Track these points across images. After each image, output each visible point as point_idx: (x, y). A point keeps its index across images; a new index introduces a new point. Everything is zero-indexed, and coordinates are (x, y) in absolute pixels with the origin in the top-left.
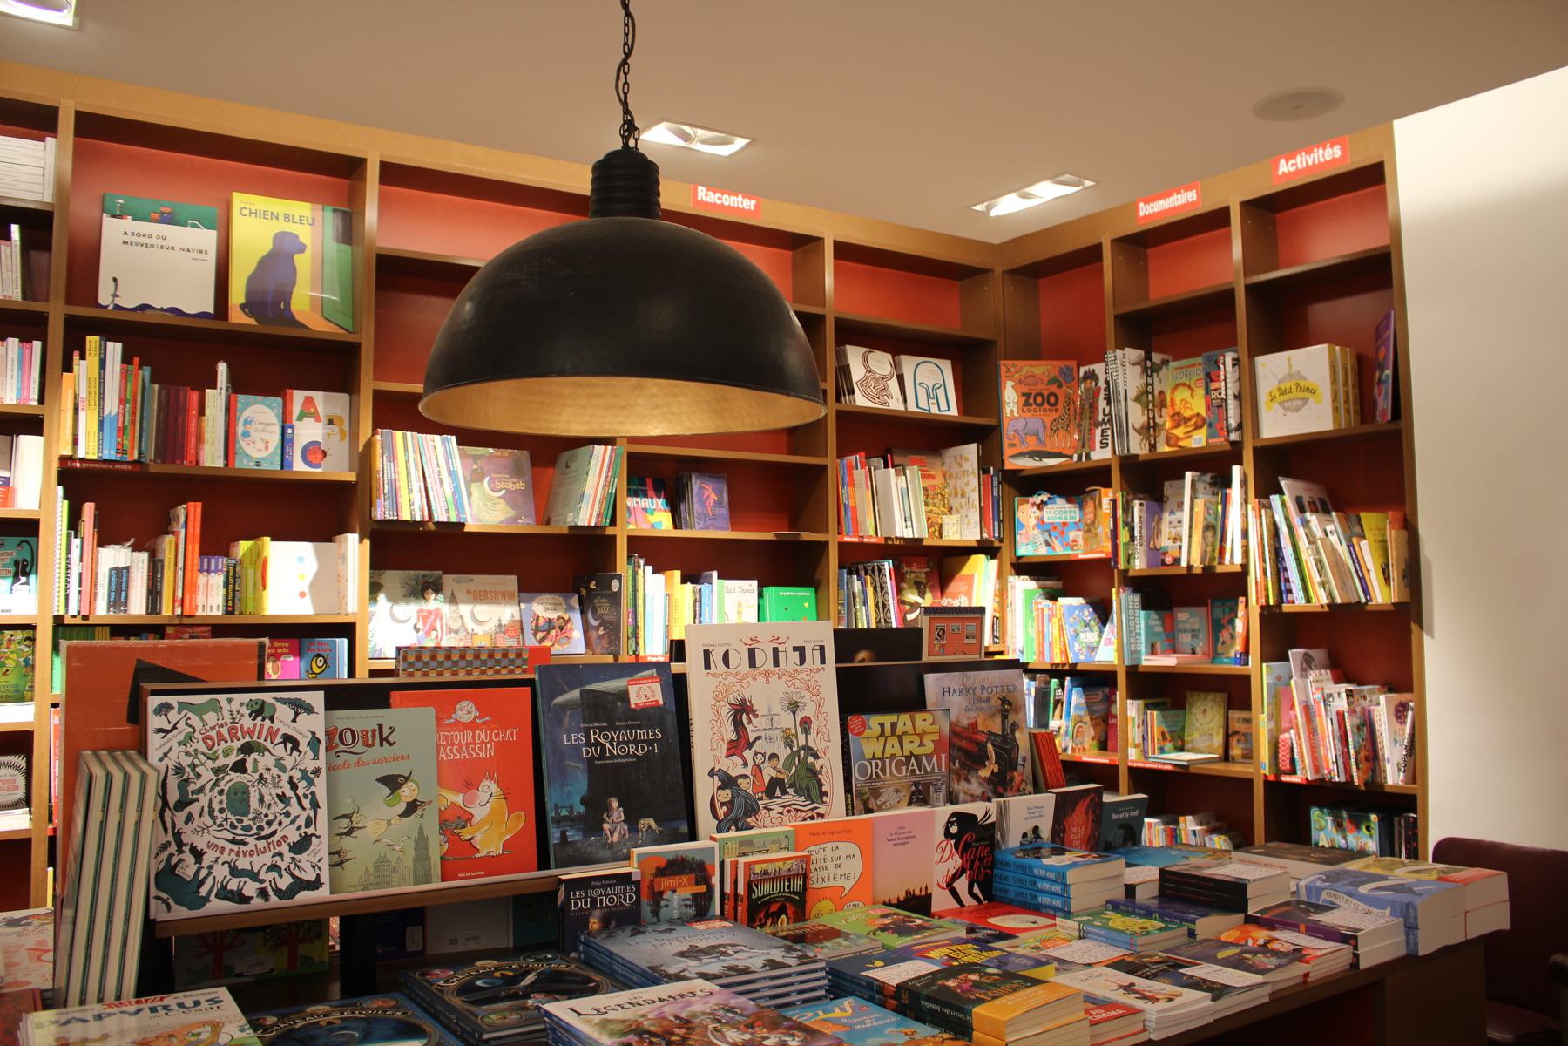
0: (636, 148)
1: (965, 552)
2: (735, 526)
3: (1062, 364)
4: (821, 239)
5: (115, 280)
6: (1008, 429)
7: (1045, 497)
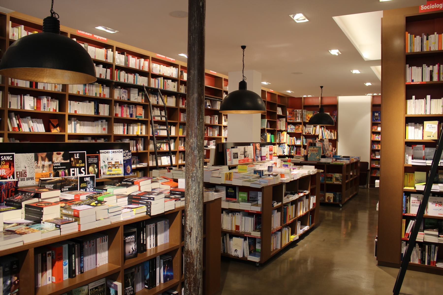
0: (55, 17)
1: (282, 131)
2: (270, 128)
3: (293, 109)
4: (149, 57)
5: (322, 87)
6: (288, 117)
7: (291, 125)
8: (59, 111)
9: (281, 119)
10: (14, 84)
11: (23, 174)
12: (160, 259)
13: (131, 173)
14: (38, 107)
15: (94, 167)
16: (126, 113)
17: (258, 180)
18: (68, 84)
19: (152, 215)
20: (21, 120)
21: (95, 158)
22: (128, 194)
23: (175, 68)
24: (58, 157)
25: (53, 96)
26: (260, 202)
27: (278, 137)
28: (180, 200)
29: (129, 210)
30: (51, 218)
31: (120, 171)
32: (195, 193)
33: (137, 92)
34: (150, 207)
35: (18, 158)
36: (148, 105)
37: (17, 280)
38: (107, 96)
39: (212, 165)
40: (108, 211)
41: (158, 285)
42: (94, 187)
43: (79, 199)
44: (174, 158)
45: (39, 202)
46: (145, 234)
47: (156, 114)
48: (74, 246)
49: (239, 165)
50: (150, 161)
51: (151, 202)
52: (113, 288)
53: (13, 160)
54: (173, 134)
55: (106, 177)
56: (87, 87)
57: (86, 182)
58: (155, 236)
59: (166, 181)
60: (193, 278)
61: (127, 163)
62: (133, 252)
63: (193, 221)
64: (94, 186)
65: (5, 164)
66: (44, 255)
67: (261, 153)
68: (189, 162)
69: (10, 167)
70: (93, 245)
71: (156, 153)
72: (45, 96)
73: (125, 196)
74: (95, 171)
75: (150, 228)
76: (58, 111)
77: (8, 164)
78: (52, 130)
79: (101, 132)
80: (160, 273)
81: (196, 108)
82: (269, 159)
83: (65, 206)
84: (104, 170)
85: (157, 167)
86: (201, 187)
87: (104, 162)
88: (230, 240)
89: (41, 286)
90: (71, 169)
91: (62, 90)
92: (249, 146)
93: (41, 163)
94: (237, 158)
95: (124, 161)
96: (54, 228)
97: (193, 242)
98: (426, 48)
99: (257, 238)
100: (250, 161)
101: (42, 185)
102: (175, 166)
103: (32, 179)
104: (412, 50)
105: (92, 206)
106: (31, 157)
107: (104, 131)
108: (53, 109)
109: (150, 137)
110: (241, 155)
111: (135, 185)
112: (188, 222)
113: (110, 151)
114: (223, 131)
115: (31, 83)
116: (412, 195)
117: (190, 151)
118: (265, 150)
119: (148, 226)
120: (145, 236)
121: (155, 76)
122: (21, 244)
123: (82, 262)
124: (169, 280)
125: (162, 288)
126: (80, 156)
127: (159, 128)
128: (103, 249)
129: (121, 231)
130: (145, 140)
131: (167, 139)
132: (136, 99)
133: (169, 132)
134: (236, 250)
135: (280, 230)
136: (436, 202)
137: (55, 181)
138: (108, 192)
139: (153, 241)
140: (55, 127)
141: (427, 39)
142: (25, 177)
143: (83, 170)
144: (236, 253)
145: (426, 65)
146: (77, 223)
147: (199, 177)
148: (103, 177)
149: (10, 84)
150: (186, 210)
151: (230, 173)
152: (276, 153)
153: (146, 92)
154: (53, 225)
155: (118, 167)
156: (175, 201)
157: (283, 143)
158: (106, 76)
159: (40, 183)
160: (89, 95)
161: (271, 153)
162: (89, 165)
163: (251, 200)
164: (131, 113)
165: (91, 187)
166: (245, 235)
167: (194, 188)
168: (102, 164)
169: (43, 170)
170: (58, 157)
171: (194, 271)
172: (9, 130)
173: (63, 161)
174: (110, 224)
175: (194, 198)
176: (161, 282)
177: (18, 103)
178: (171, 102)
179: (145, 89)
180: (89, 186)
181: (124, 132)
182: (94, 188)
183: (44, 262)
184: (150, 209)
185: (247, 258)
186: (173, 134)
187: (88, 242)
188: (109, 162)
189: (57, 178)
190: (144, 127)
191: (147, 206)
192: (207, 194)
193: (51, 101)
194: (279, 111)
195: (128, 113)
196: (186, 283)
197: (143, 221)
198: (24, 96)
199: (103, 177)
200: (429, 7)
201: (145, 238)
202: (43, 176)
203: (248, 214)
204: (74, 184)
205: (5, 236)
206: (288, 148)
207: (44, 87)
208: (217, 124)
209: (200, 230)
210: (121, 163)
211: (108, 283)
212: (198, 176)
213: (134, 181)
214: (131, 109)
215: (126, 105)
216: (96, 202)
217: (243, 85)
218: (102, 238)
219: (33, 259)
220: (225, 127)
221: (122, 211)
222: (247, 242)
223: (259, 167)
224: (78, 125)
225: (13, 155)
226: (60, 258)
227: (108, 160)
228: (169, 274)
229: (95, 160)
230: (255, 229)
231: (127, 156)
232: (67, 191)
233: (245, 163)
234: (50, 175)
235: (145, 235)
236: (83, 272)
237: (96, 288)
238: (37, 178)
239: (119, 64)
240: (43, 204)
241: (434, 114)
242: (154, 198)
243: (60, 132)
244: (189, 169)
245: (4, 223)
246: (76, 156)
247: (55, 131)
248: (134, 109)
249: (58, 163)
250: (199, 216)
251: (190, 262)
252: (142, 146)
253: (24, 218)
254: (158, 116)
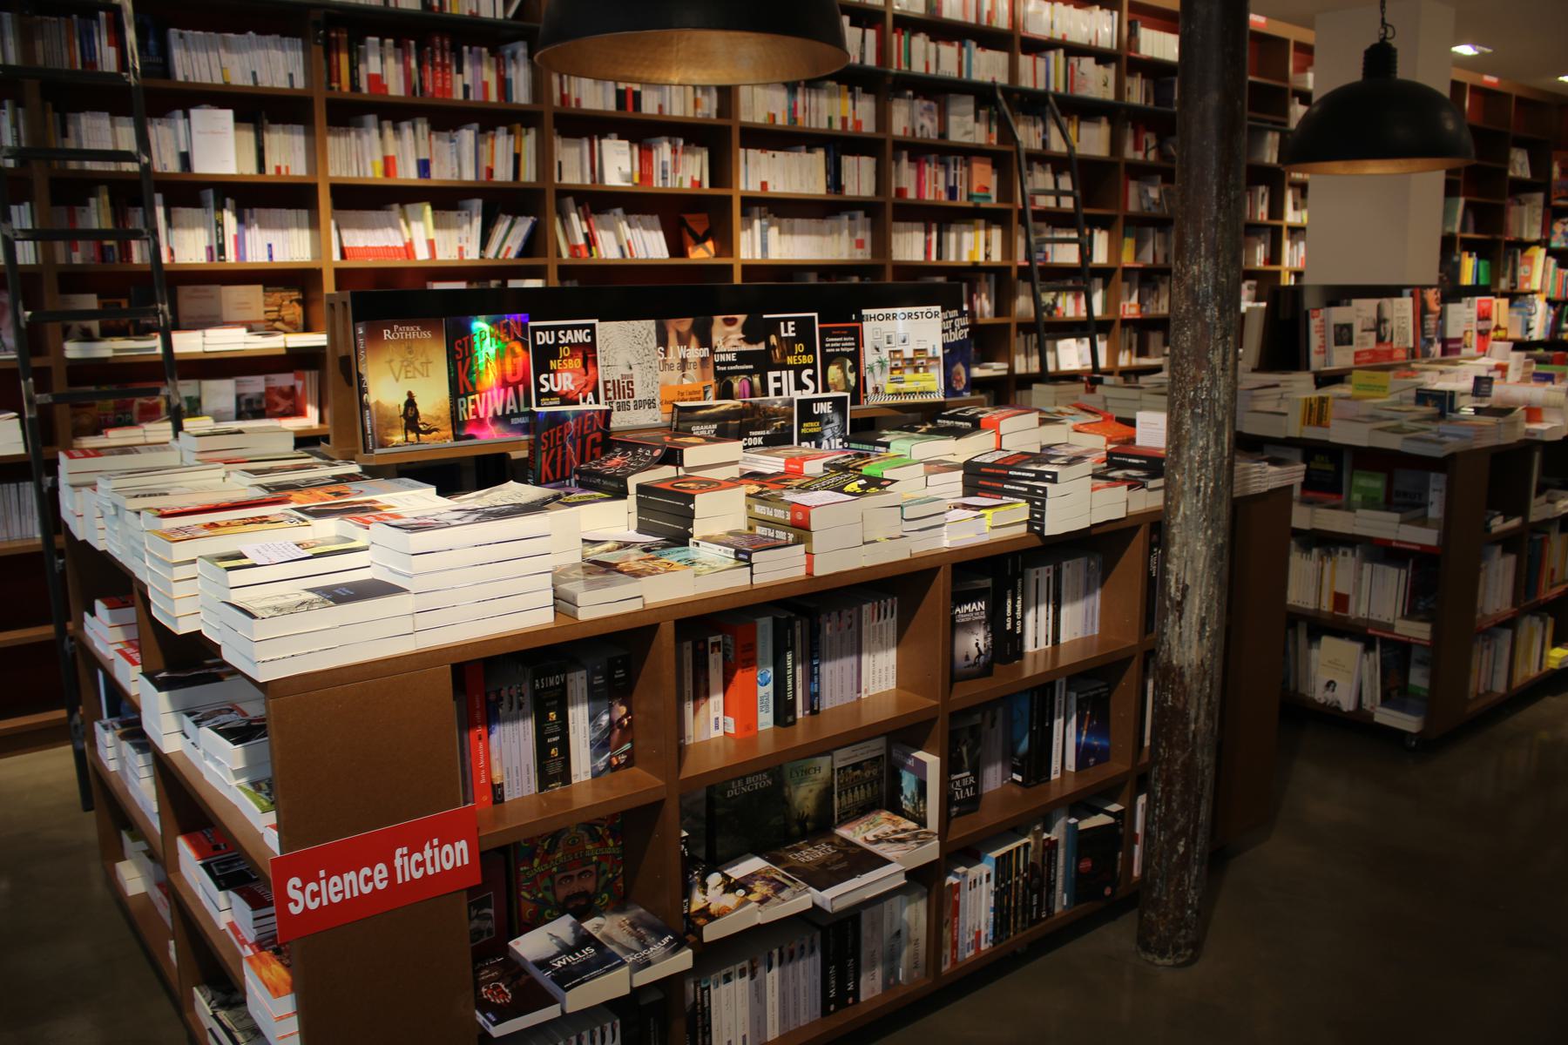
1: (1525, 245)
2: (1476, 232)
8: (712, 185)
9: (1523, 197)
10: (569, 103)
11: (623, 389)
12: (1068, 689)
13: (966, 389)
14: (645, 176)
15: (843, 368)
16: (933, 186)
17: (1434, 427)
18: (738, 86)
19: (1046, 534)
20: (594, 219)
21: (847, 336)
22: (961, 460)
23: (1106, 12)
24: (730, 333)
25: (689, 133)
26: (1435, 512)
27: (1506, 269)
28: (1143, 487)
29: (970, 513)
30: (718, 530)
31: (930, 384)
32: (1203, 463)
33: (971, 107)
34: (1043, 506)
35: (607, 337)
36: (1011, 153)
37: (626, 716)
38: (868, 127)
39: (1254, 370)
40: (902, 513)
41: (1055, 776)
42: (846, 436)
43: (799, 473)
44: (1102, 347)
45: (678, 477)
46: (1019, 598)
47: (1040, 186)
48: (790, 624)
49: (1356, 369)
50: (1019, 354)
51: (1044, 489)
52: (911, 770)
53: (593, 344)
54: (1100, 256)
55: (882, 402)
56: (800, 99)
57: (819, 417)
58: (1054, 609)
59: (1091, 418)
60: (1183, 764)
61: (953, 354)
62: (978, 657)
63: (1192, 562)
64: (845, 431)
65: (571, 356)
66: (701, 646)
67: (1442, 328)
68: (1183, 348)
69: (585, 366)
70: (850, 626)
71: (1042, 327)
72: (665, 135)
73: (953, 468)
74: (847, 381)
75: (1037, 580)
76: (706, 185)
77: (580, 354)
78: (690, 249)
79: (850, 255)
80: (1066, 737)
81: (1214, 147)
82: (1473, 351)
83: (760, 493)
84: (878, 379)
85: (1044, 377)
86: (1226, 441)
87: (877, 349)
88: (1310, 647)
89: (692, 741)
90: (771, 375)
91: (720, 113)
92: (1396, 300)
93: (676, 352)
94: (1350, 342)
95: (945, 346)
96: (732, 562)
97: (1190, 635)
99: (1416, 644)
100: (1400, 355)
101: (682, 426)
102: (1109, 373)
103: (650, 403)
105: (849, 493)
106: (645, 332)
107: (859, 251)
108: (693, 182)
109: (1021, 269)
110: (1364, 330)
111: (984, 430)
112: (1173, 567)
113: (898, 310)
114: (1286, 245)
115: (621, 96)
117: (1188, 306)
118: (1462, 317)
119: (1032, 574)
120: (1019, 606)
121: (1037, 47)
122: (635, 606)
123: (816, 679)
124: (1096, 763)
125: (1070, 787)
126: (797, 329)
127: (1049, 236)
128: (881, 642)
129: (942, 583)
130: (1002, 280)
131: (1080, 277)
132: (967, 133)
133: (1086, 252)
134: (1330, 685)
135: (1510, 623)
137: (722, 412)
138: (893, 451)
139: (1047, 625)
140: (700, 241)
142: (629, 397)
143: (809, 376)
144: (1329, 695)
146: (801, 548)
147: (1222, 402)
148: (872, 400)
149: (556, 101)
150: (1169, 522)
151: (1323, 400)
152: (1505, 329)
153: (1005, 107)
154: (726, 552)
155: (926, 369)
156: (1130, 488)
157: (1526, 294)
158: (862, 55)
159: (675, 418)
160: (807, 125)
161: (1483, 326)
162: (828, 360)
163: (1405, 503)
164: (952, 184)
165: (834, 437)
166: (1370, 631)
167: (1201, 443)
168: (869, 357)
169: (683, 376)
170: (730, 333)
171: (1187, 741)
172: (559, 255)
173: (745, 347)
174: (908, 557)
175: (1199, 481)
176: (1067, 768)
177: (582, 164)
178: (1093, 140)
179: (1000, 96)
180: (828, 433)
181: (927, 252)
182: (846, 439)
183: (701, 667)
184: (1043, 515)
185: (1371, 716)
186: (1100, 256)
187: (834, 614)
188: (895, 352)
189: (728, 404)
190: (996, 234)
191: (1030, 501)
192: (1244, 469)
193: (684, 152)
194: (1520, 165)
195: (941, 187)
196: (1156, 780)
197: (1014, 555)
198: (600, 138)
199: (872, 400)
201: (1019, 614)
202: (685, 397)
203: (1383, 552)
204: (782, 425)
205: (590, 578)
206: (1548, 312)
207: (661, 107)
208: (1265, 218)
209: (1216, 596)
210: (934, 353)
211: (894, 755)
212: (1218, 400)
213: (980, 416)
214: (952, 171)
215: (933, 157)
216: (863, 482)
217: (1380, 58)
218: (879, 603)
219: (673, 654)
220: (1296, 231)
221: (946, 516)
222: (1376, 656)
223: (1437, 380)
224: (773, 232)
225: (594, 325)
226: (750, 662)
227: (889, 343)
228: (1096, 743)
229: (846, 344)
230: (1411, 613)
231: (953, 331)
232: (757, 446)
233: (1380, 361)
234: (706, 393)
235: (1019, 602)
236: (818, 712)
237: (856, 766)
238: (667, 403)
239: (906, 9)
240: (691, 485)
242: (1055, 474)
243: (717, 255)
244: (1182, 375)
245: (584, 540)
246: (786, 331)
247: (701, 254)
248: (961, 172)
249: (727, 352)
250: (1216, 546)
251: (1173, 708)
252: (990, 302)
253: (636, 527)
254: (1046, 193)
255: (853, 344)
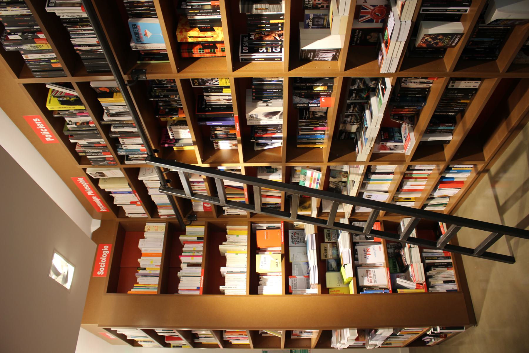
98: (156, 271)
104: (156, 287)
116: (360, 284)
136: (365, 255)
141: (145, 269)
145: (180, 271)
200: (103, 266)
241: (246, 263)
255: (227, 196)
